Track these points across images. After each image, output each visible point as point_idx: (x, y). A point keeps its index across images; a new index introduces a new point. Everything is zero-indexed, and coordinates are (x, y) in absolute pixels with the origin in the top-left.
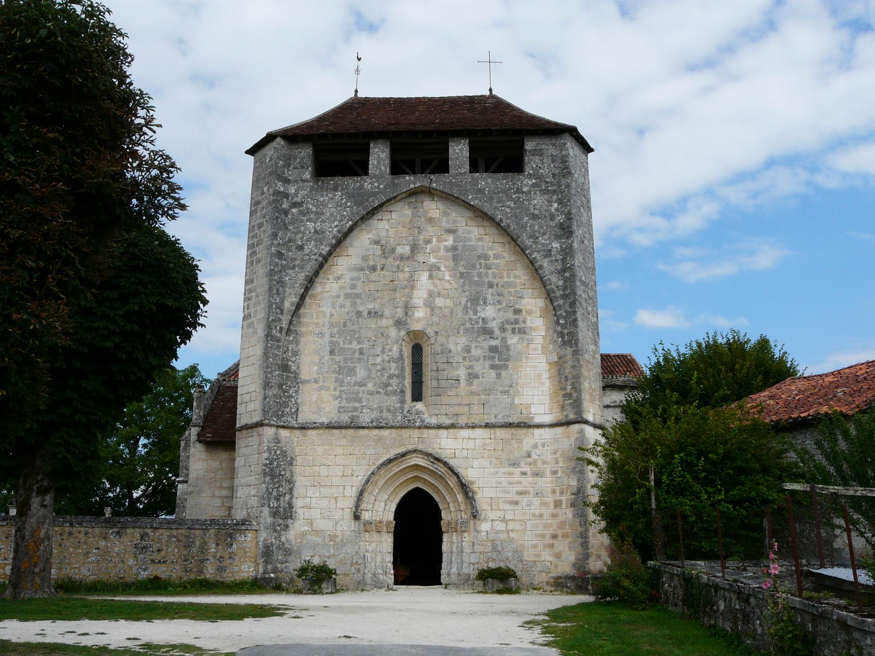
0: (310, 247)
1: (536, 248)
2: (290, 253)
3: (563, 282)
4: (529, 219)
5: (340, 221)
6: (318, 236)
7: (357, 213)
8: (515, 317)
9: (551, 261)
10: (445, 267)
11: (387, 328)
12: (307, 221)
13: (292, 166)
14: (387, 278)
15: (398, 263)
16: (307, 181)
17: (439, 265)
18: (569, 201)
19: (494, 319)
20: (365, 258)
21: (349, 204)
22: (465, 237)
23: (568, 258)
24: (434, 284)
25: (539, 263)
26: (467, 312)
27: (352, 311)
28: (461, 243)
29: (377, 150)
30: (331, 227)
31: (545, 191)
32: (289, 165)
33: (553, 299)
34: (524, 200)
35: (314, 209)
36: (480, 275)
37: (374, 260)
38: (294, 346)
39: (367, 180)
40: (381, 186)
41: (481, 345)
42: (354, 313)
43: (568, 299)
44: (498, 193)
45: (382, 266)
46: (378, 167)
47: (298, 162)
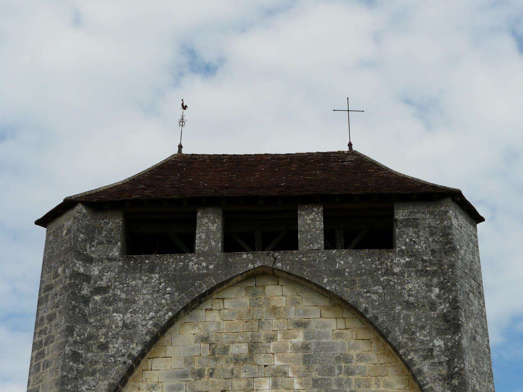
1: (412, 346)
2: (90, 354)
4: (403, 309)
5: (156, 312)
6: (128, 332)
9: (433, 364)
10: (294, 372)
12: (113, 312)
13: (96, 241)
15: (232, 366)
17: (286, 369)
18: (454, 285)
22: (319, 332)
23: (456, 360)
25: (417, 367)
28: (315, 340)
29: (206, 220)
30: (145, 320)
32: (92, 239)
34: (395, 283)
35: (123, 296)
39: (193, 258)
40: (211, 267)
44: (362, 275)
45: (211, 371)
46: (207, 241)
47: (103, 235)
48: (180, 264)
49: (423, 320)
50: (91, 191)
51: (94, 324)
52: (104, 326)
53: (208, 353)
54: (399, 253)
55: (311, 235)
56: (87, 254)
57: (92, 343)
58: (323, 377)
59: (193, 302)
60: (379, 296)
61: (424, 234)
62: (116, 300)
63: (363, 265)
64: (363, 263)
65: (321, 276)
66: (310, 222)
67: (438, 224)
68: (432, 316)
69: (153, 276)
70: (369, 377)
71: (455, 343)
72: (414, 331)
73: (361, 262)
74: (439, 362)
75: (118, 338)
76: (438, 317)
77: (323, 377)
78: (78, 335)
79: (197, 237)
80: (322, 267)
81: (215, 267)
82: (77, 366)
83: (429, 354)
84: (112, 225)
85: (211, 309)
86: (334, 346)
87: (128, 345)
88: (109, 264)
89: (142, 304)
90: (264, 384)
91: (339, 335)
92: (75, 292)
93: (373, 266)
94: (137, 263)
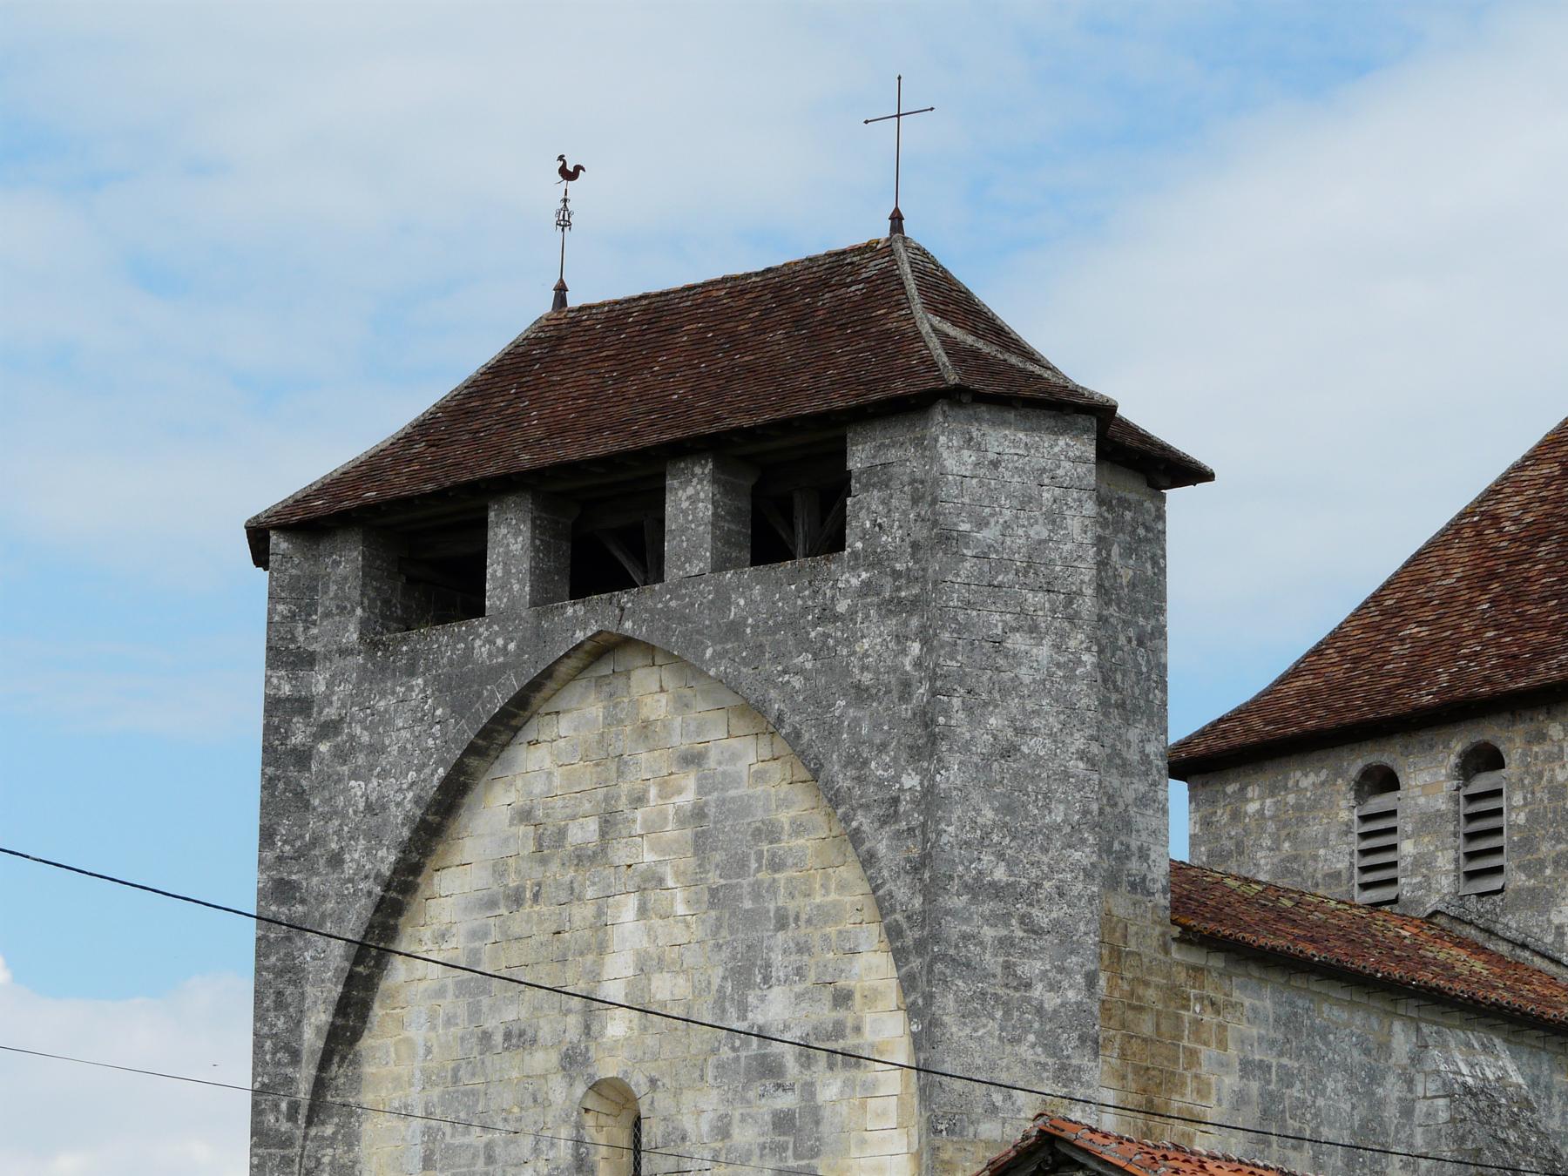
0: (355, 855)
1: (861, 797)
2: (315, 880)
5: (419, 771)
6: (373, 821)
7: (455, 740)
8: (835, 1015)
10: (678, 874)
11: (544, 1077)
12: (350, 779)
17: (661, 869)
21: (439, 712)
22: (724, 773)
24: (649, 931)
27: (472, 1034)
29: (504, 531)
30: (400, 790)
31: (894, 606)
32: (311, 608)
36: (757, 896)
37: (518, 872)
38: (339, 1151)
39: (481, 630)
41: (754, 1111)
42: (474, 1040)
44: (777, 628)
46: (504, 586)
47: (332, 594)
48: (458, 647)
50: (311, 485)
51: (320, 810)
54: (849, 562)
56: (299, 648)
57: (317, 853)
58: (729, 882)
59: (486, 733)
60: (805, 679)
61: (900, 502)
63: (780, 604)
64: (779, 600)
66: (687, 504)
69: (414, 683)
70: (812, 871)
72: (867, 758)
73: (778, 595)
74: (909, 829)
76: (915, 714)
77: (729, 882)
78: (285, 842)
79: (488, 576)
81: (518, 646)
82: (289, 910)
84: (345, 567)
85: (537, 741)
86: (751, 806)
87: (374, 852)
88: (342, 664)
89: (395, 753)
90: (624, 909)
91: (759, 777)
92: (272, 746)
93: (800, 602)
94: (388, 654)
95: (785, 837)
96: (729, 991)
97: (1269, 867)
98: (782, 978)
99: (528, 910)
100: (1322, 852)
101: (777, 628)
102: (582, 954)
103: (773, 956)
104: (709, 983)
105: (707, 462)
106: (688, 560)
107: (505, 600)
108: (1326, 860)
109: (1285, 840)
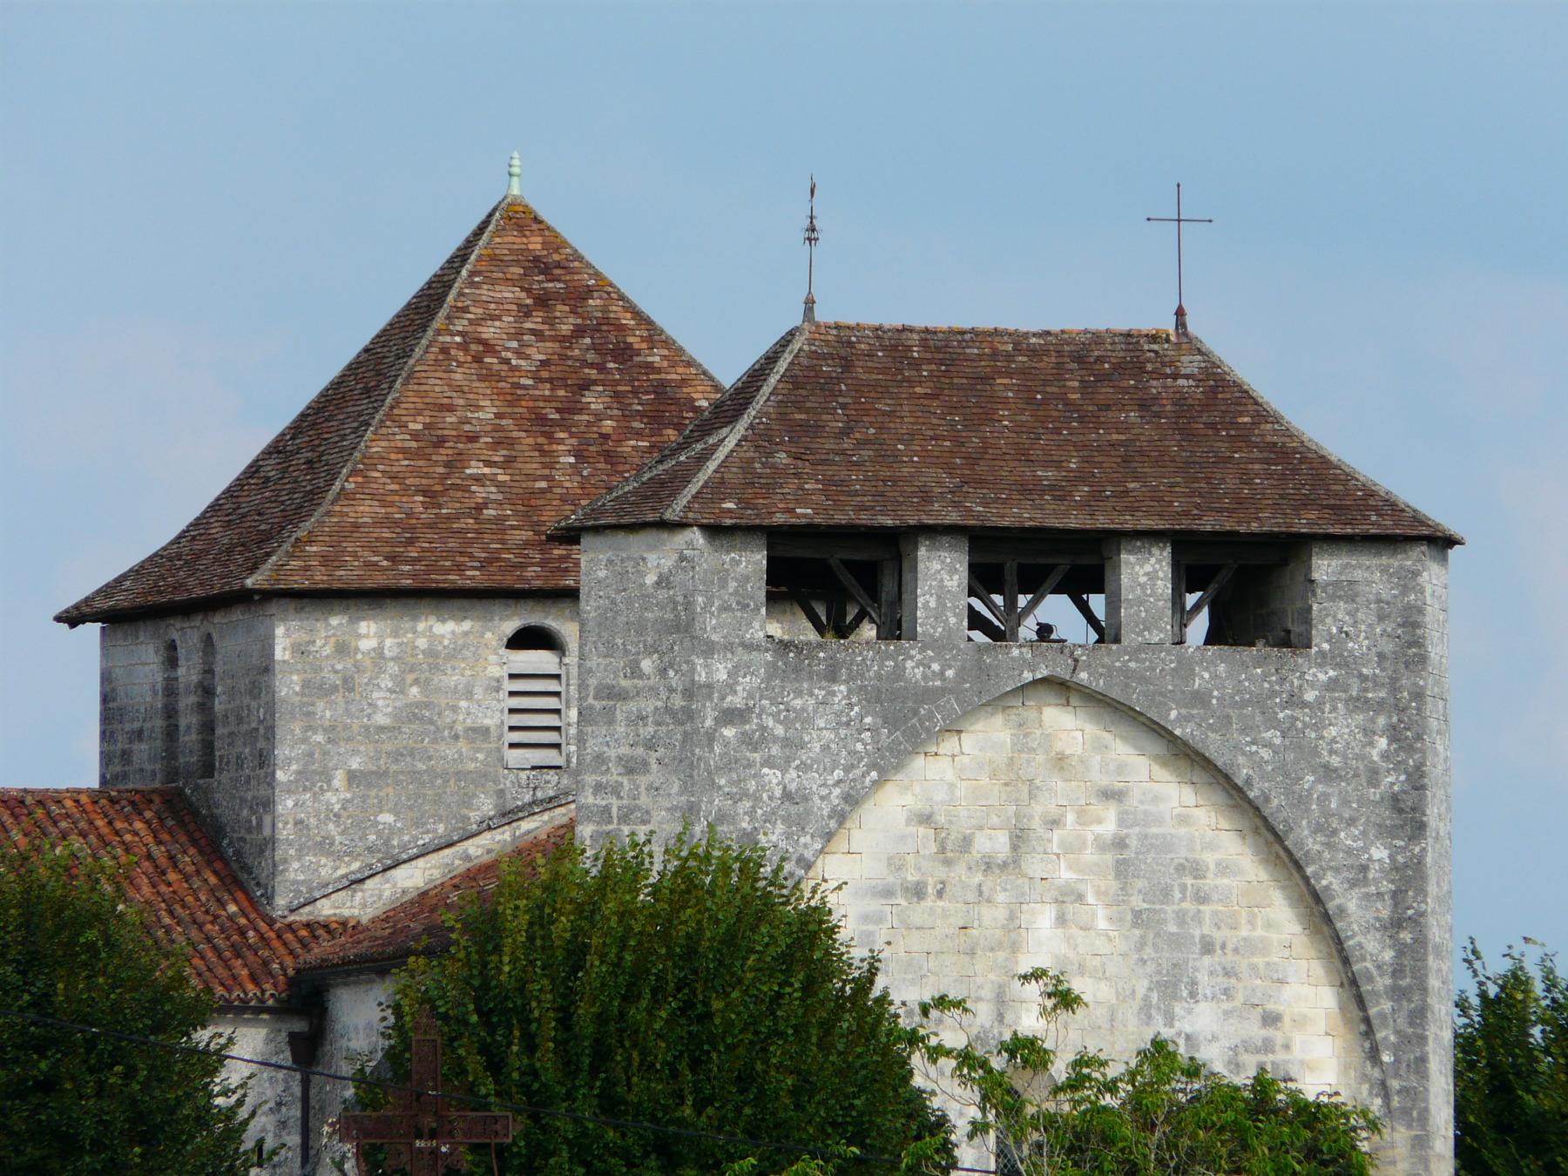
1: (1330, 860)
3: (1392, 953)
4: (1318, 781)
6: (793, 809)
7: (890, 749)
9: (1367, 896)
10: (1098, 893)
12: (762, 766)
13: (716, 604)
14: (952, 920)
15: (978, 878)
16: (757, 648)
17: (1081, 887)
18: (1419, 737)
19: (1215, 1038)
20: (896, 863)
21: (868, 720)
22: (1145, 812)
23: (1410, 893)
24: (1069, 939)
25: (1337, 901)
26: (1150, 1017)
28: (1137, 829)
29: (936, 566)
30: (824, 785)
31: (1358, 704)
33: (1367, 998)
34: (1306, 725)
35: (780, 731)
36: (1181, 919)
39: (913, 652)
40: (950, 673)
43: (1405, 1003)
44: (1243, 704)
45: (939, 886)
46: (939, 615)
47: (731, 590)
49: (1354, 805)
51: (727, 790)
52: (745, 794)
53: (933, 848)
55: (1146, 611)
61: (1366, 616)
62: (765, 738)
64: (1246, 679)
65: (1166, 704)
67: (1395, 597)
68: (1372, 798)
71: (1411, 860)
75: (775, 822)
76: (1382, 798)
77: (1152, 906)
79: (919, 605)
80: (1167, 684)
83: (1361, 876)
89: (818, 750)
93: (1266, 685)
95: (1210, 875)
96: (1155, 1000)
97: (390, 709)
98: (1209, 995)
99: (930, 904)
100: (463, 704)
101: (1243, 704)
102: (992, 950)
103: (1199, 975)
104: (1134, 991)
105: (1165, 547)
106: (1147, 629)
107: (940, 630)
108: (469, 714)
109: (411, 685)
